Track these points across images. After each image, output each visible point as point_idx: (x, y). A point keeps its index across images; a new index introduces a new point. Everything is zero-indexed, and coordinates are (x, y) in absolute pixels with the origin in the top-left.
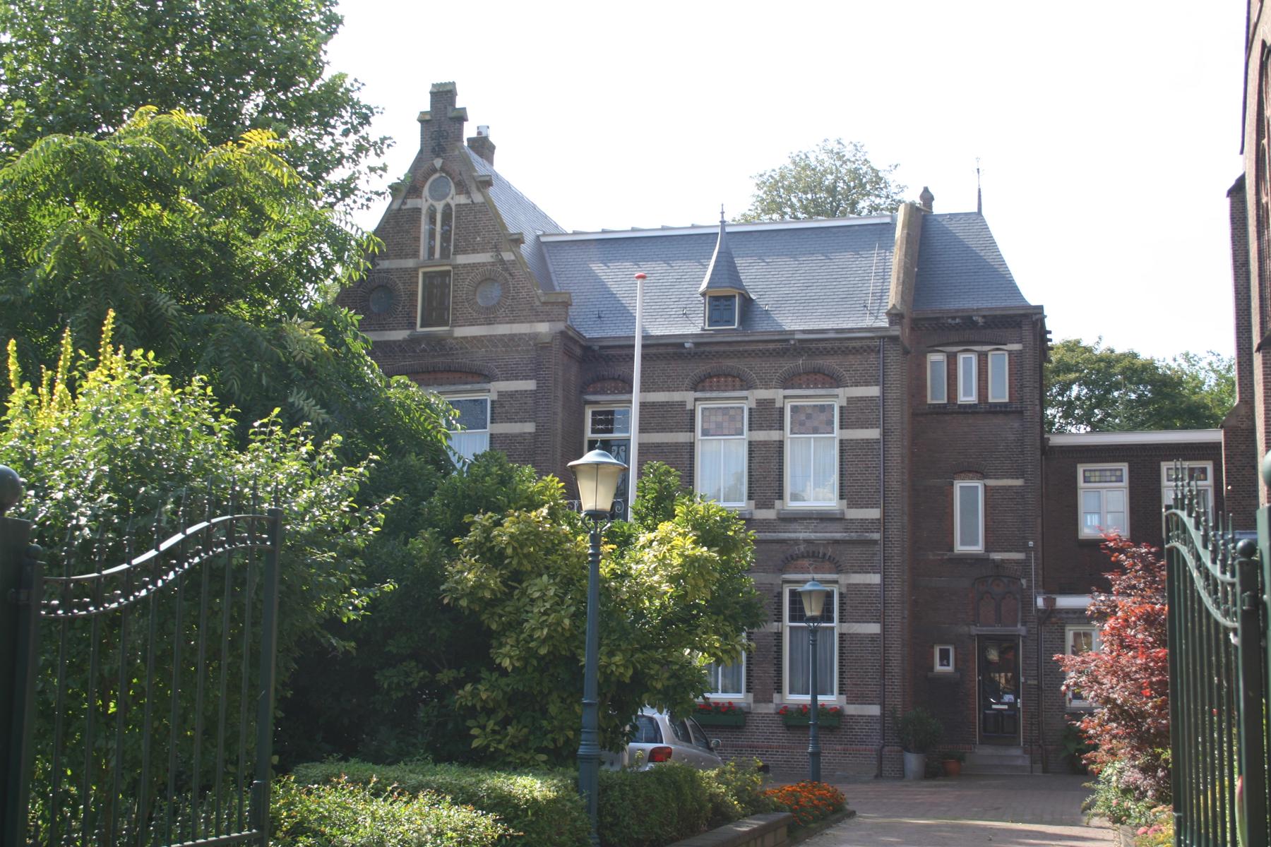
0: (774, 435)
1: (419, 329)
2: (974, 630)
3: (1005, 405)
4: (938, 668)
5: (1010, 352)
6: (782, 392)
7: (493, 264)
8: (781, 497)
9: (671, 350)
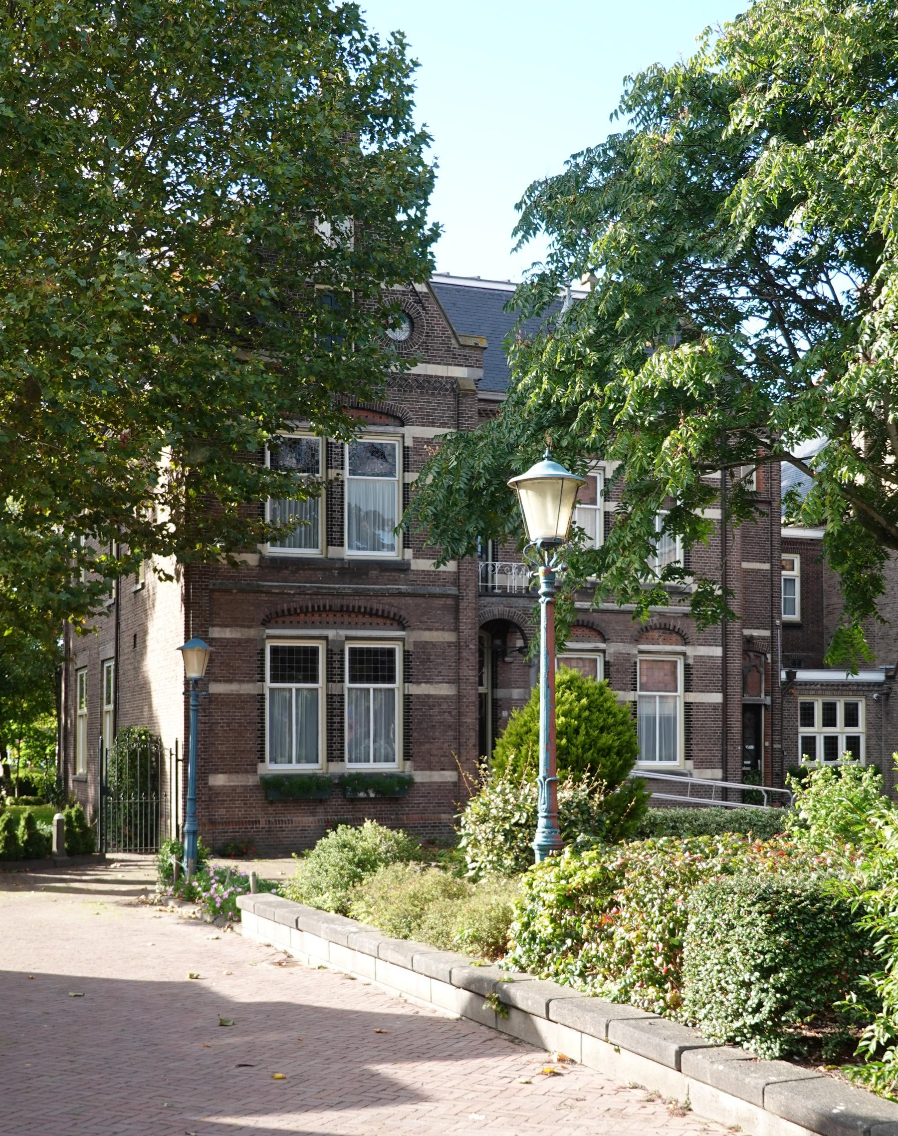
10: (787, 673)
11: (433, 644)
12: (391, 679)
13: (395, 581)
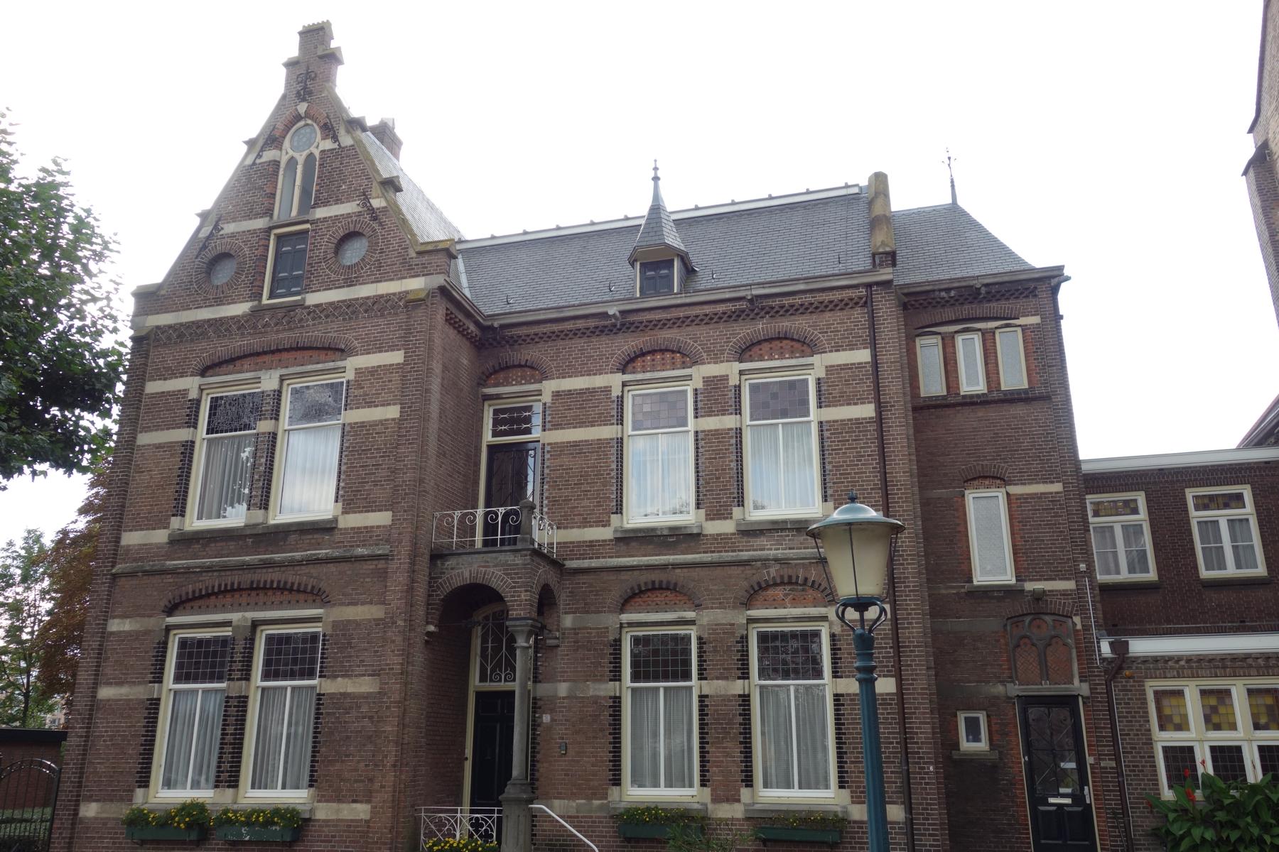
0: (729, 422)
1: (265, 301)
2: (1014, 689)
3: (1025, 391)
4: (966, 746)
5: (1024, 328)
6: (738, 366)
7: (359, 214)
8: (741, 503)
9: (592, 323)
10: (1111, 644)
11: (357, 624)
12: (686, 676)
13: (318, 545)
